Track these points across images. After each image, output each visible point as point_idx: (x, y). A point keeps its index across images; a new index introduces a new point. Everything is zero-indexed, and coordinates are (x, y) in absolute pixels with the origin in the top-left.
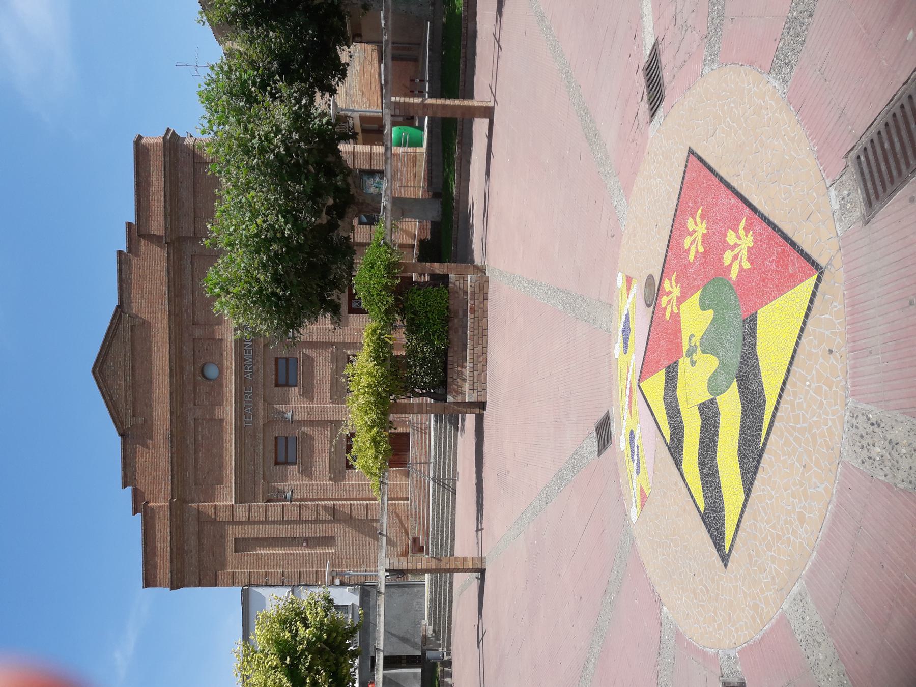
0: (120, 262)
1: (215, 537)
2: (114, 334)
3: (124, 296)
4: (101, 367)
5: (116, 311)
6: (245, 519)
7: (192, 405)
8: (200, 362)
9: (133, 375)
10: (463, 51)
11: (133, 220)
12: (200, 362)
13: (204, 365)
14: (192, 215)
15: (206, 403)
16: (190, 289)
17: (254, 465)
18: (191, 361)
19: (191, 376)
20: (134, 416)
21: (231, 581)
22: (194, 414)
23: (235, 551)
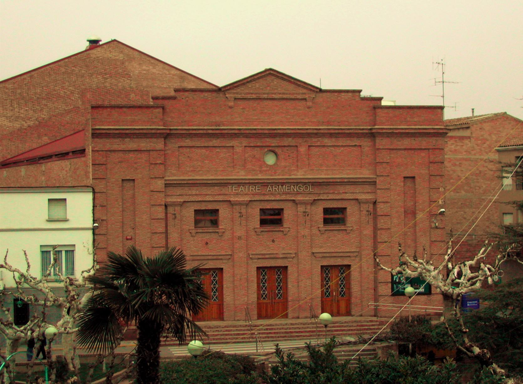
0: (354, 92)
1: (136, 163)
2: (299, 86)
3: (328, 94)
4: (270, 74)
5: (317, 88)
6: (379, 226)
7: (244, 145)
8: (278, 151)
9: (267, 99)
10: (174, 360)
11: (363, 94)
12: (278, 151)
13: (276, 154)
14: (392, 147)
15: (247, 155)
16: (336, 144)
17: (196, 195)
18: (280, 144)
19: (268, 144)
20: (235, 99)
21: (97, 176)
22: (237, 146)
23: (123, 180)
